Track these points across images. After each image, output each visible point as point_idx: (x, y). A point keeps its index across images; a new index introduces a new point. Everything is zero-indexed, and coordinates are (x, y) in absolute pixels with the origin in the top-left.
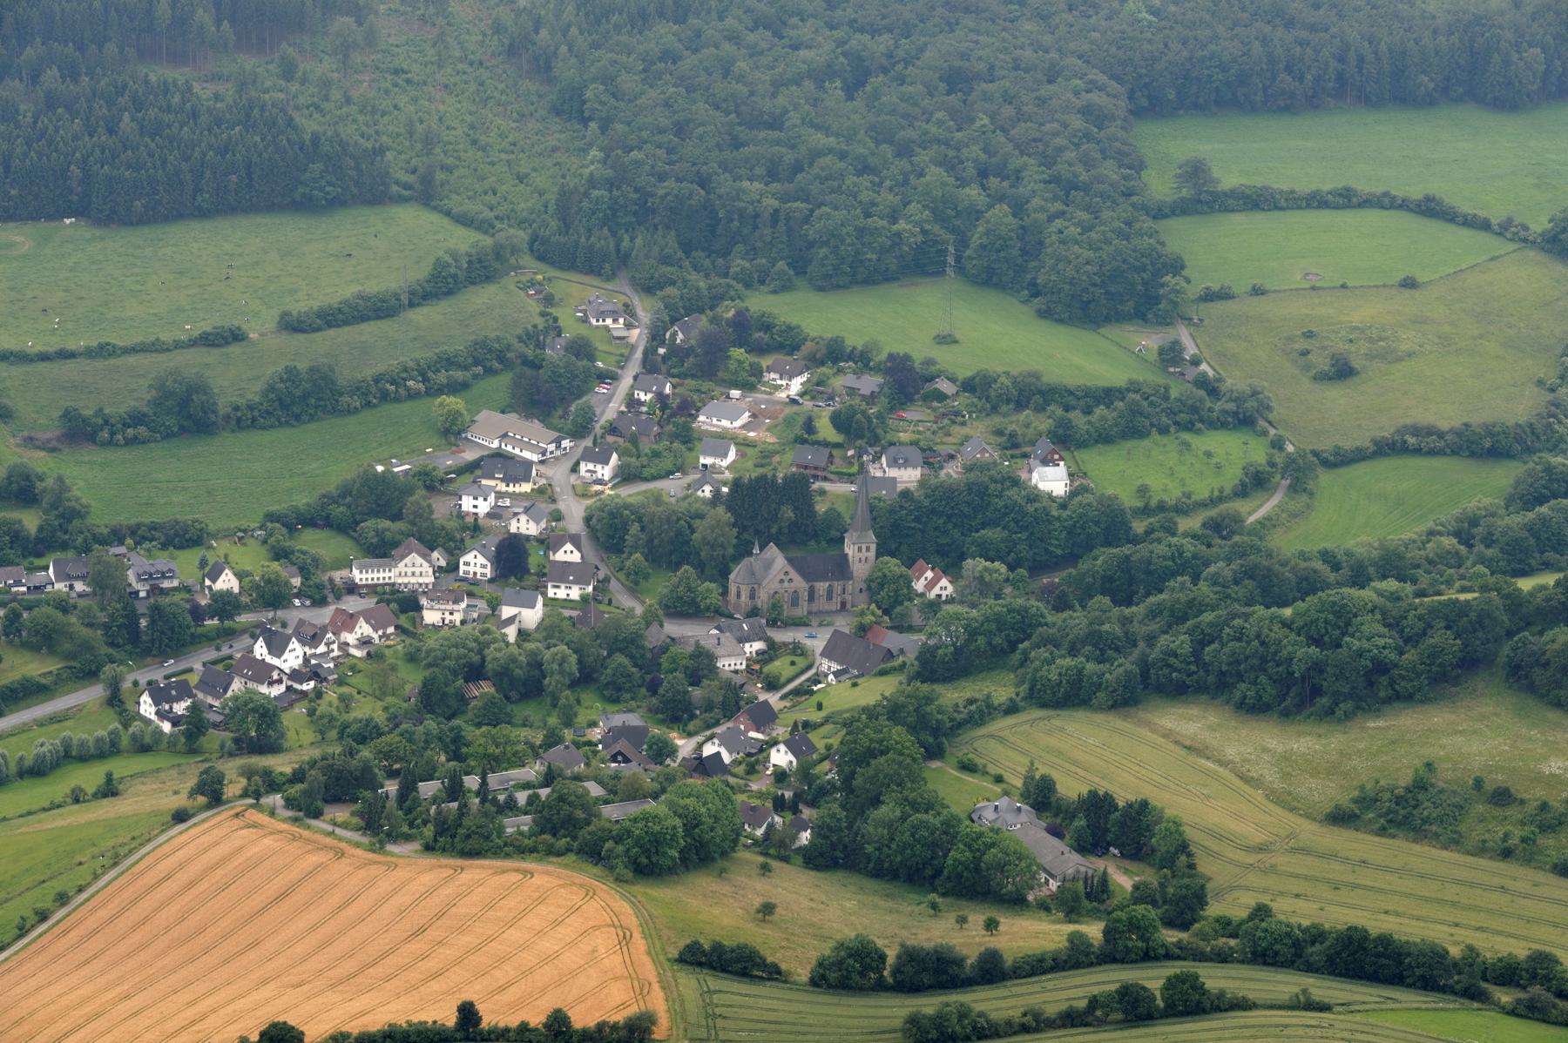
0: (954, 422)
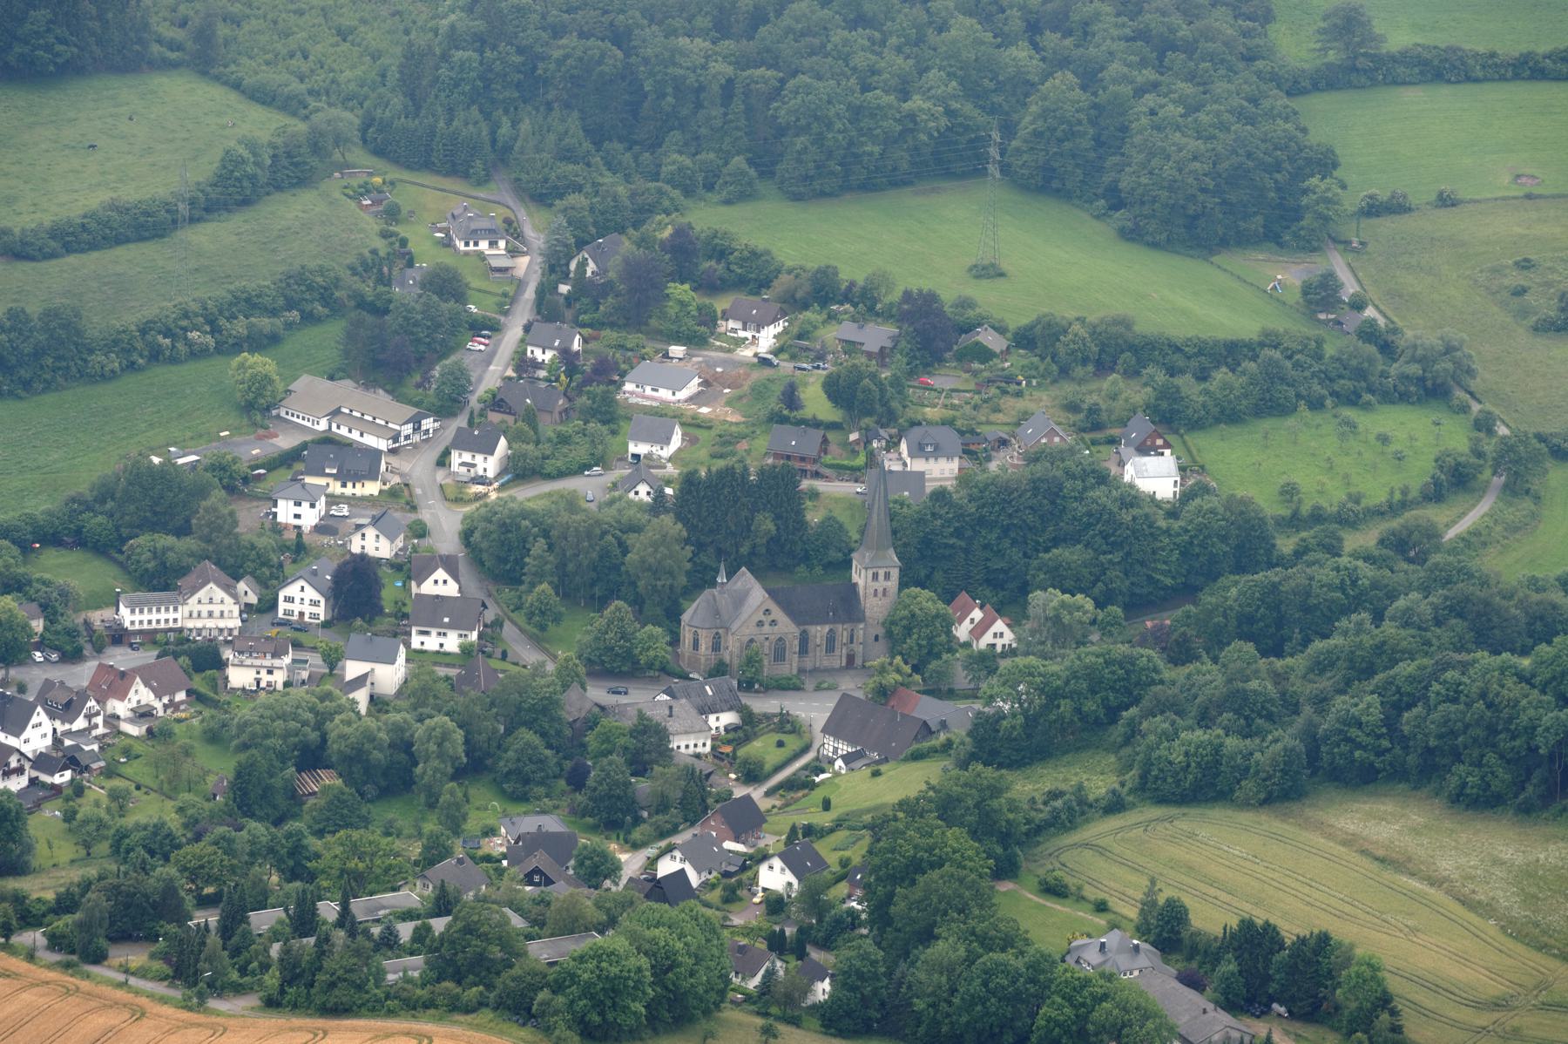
0: (1005, 392)
